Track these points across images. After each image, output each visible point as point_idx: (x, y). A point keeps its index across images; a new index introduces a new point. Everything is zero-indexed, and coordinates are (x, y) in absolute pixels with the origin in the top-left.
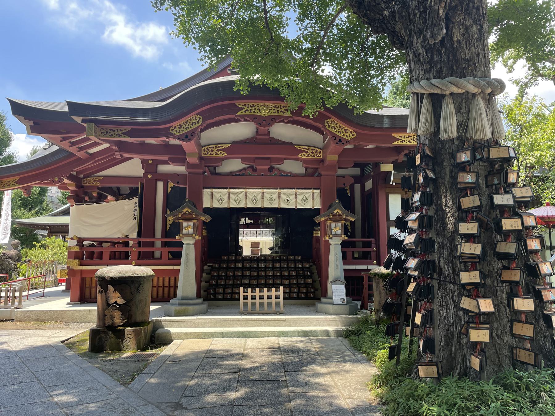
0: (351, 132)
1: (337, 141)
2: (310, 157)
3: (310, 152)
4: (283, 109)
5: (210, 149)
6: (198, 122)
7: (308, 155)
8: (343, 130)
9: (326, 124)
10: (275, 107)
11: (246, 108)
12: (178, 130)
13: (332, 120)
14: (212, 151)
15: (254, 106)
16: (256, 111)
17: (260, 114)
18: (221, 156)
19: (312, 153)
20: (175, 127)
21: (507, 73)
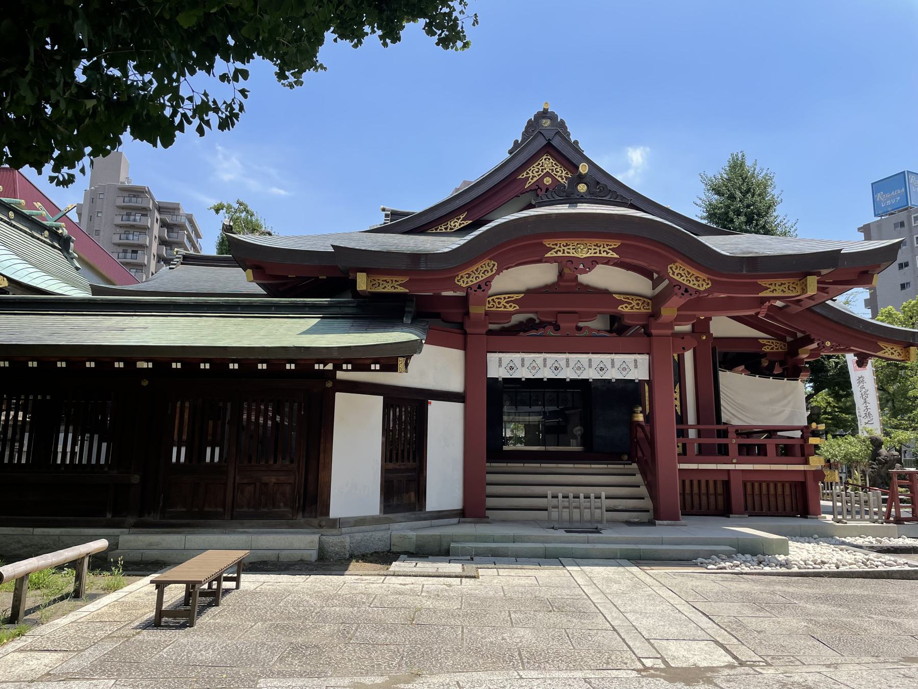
0: (704, 280)
1: (682, 291)
2: (634, 310)
3: (634, 303)
4: (606, 249)
5: (497, 301)
6: (492, 270)
7: (632, 308)
8: (693, 278)
9: (669, 270)
10: (596, 245)
11: (557, 248)
12: (466, 280)
13: (677, 264)
14: (499, 303)
15: (567, 245)
16: (571, 251)
17: (576, 255)
18: (511, 309)
19: (638, 304)
20: (462, 277)
21: (356, 46)
